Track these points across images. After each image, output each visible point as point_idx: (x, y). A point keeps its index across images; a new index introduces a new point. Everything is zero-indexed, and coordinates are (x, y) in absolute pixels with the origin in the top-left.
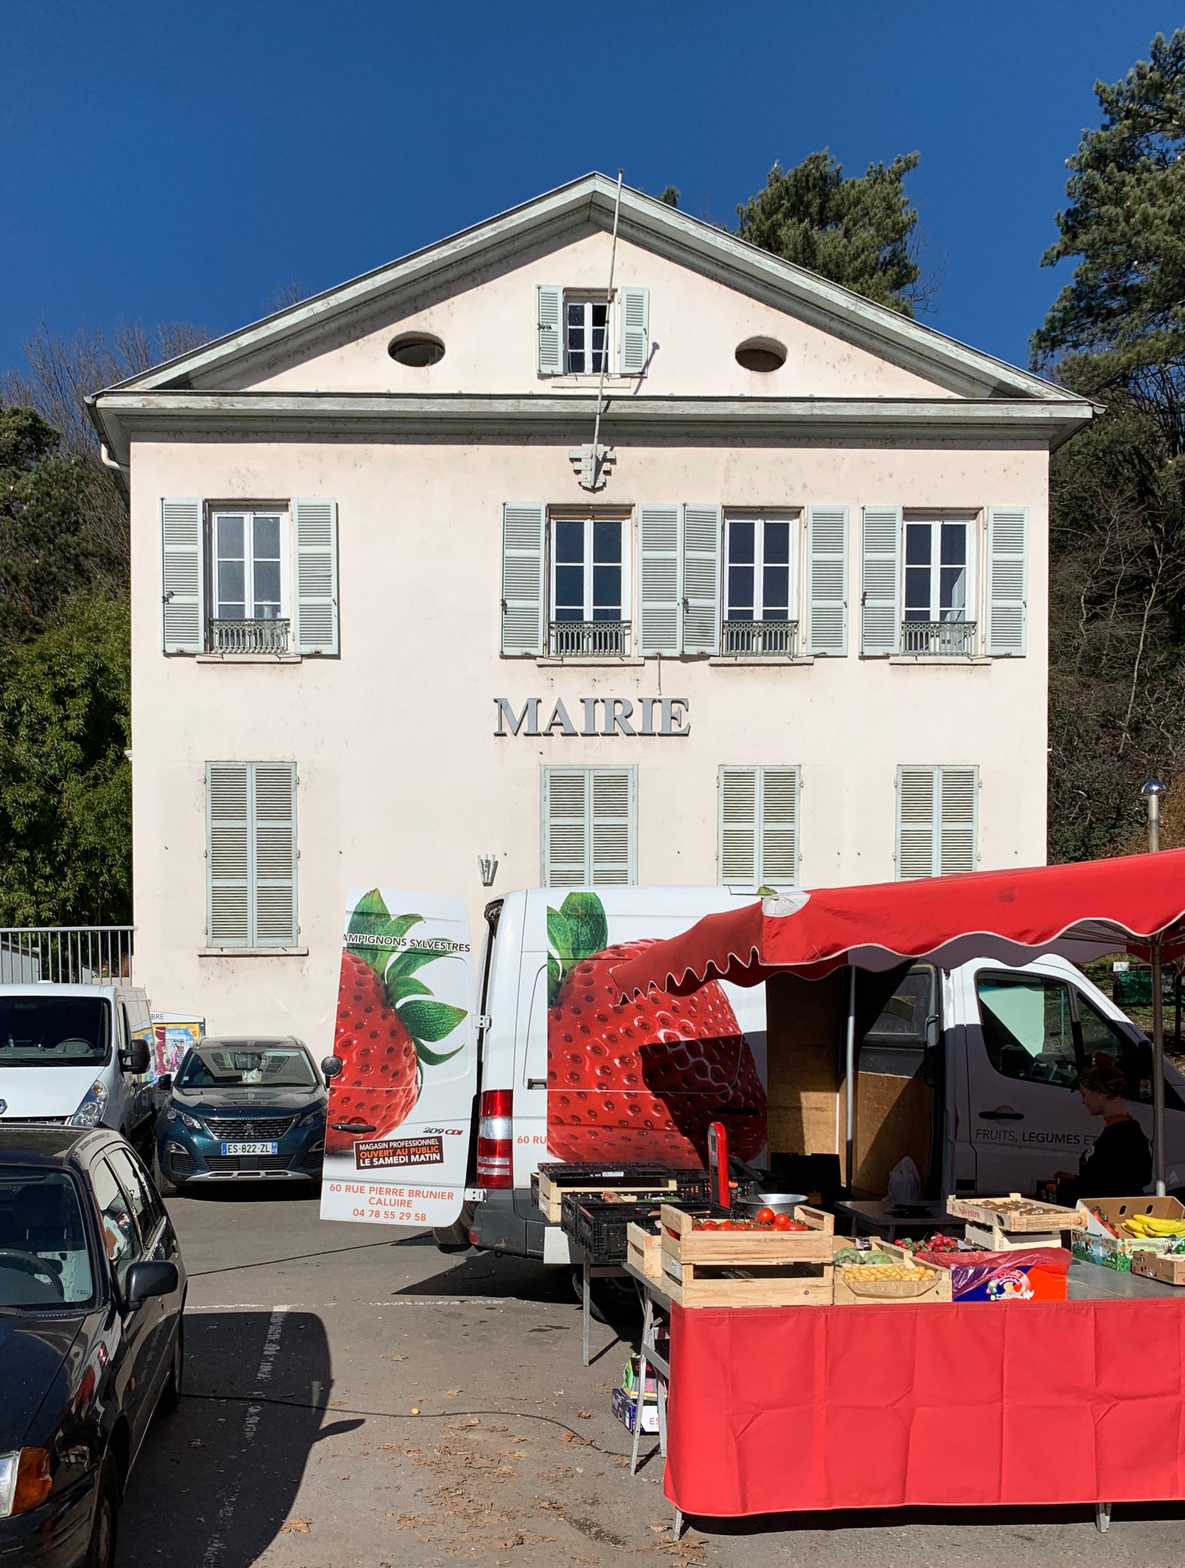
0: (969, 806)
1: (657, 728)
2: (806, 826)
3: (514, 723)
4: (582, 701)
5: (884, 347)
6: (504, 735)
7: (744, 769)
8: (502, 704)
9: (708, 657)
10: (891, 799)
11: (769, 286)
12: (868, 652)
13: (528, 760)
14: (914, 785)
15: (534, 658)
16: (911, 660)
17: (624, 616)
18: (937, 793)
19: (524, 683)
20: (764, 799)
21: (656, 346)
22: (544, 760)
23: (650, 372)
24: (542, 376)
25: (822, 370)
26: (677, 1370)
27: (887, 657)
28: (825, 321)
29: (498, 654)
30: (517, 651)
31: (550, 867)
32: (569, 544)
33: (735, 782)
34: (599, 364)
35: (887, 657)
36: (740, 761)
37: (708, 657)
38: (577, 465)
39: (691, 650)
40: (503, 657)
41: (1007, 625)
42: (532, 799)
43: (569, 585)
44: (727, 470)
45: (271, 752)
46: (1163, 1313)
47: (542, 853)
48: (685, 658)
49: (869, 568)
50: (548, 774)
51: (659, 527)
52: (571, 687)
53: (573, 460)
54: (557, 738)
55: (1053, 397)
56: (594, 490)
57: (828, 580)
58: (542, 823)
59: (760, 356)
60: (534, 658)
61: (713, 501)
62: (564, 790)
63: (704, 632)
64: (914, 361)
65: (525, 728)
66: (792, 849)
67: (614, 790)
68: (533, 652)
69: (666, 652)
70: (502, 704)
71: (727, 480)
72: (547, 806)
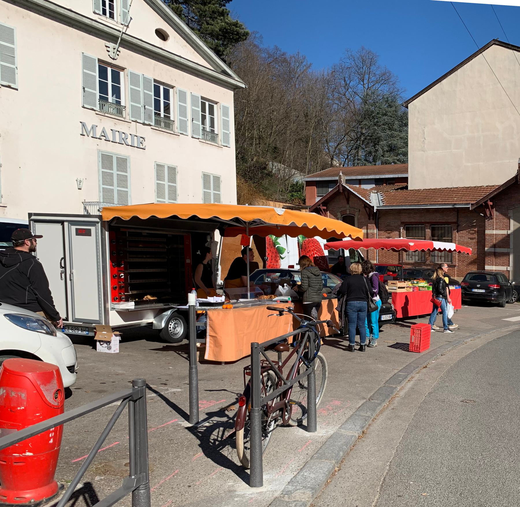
0: (219, 187)
1: (118, 141)
2: (179, 185)
3: (85, 131)
4: (112, 130)
5: (195, 47)
6: (84, 135)
7: (162, 164)
8: (83, 125)
9: (151, 126)
10: (200, 182)
11: (165, 15)
12: (86, 106)
13: (93, 148)
14: (206, 177)
15: (95, 111)
16: (204, 141)
17: (172, 118)
18: (211, 181)
19: (91, 119)
20: (167, 174)
21: (131, 19)
22: (99, 147)
23: (129, 25)
24: (95, 13)
25: (176, 46)
26: (189, 356)
27: (199, 139)
28: (181, 33)
29: (81, 105)
30: (89, 107)
31: (102, 186)
32: (103, 73)
33: (159, 167)
34: (112, 16)
35: (199, 139)
36: (161, 162)
37: (151, 126)
38: (108, 49)
39: (147, 122)
40: (83, 107)
41: (226, 136)
42: (95, 161)
43: (157, 103)
44: (154, 68)
45: (216, 173)
46: (519, 332)
47: (99, 181)
48: (144, 124)
49: (193, 111)
50: (100, 153)
51: (134, 79)
52: (107, 124)
53: (106, 46)
54: (103, 141)
55: (236, 79)
56: (114, 59)
57: (183, 111)
58: (99, 170)
59: (162, 35)
60: (95, 111)
61: (151, 76)
62: (106, 160)
63: (150, 118)
64: (203, 55)
65: (91, 135)
66: (176, 191)
67: (123, 163)
68: (95, 108)
69: (138, 121)
70: (83, 125)
71: (154, 71)
72: (100, 164)
